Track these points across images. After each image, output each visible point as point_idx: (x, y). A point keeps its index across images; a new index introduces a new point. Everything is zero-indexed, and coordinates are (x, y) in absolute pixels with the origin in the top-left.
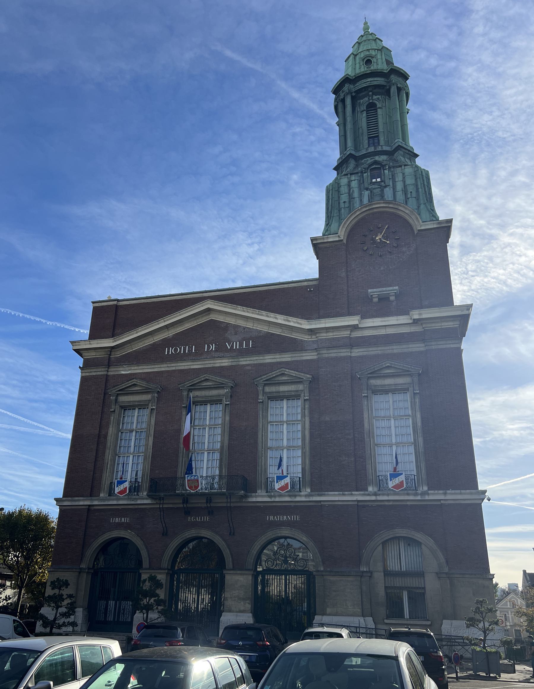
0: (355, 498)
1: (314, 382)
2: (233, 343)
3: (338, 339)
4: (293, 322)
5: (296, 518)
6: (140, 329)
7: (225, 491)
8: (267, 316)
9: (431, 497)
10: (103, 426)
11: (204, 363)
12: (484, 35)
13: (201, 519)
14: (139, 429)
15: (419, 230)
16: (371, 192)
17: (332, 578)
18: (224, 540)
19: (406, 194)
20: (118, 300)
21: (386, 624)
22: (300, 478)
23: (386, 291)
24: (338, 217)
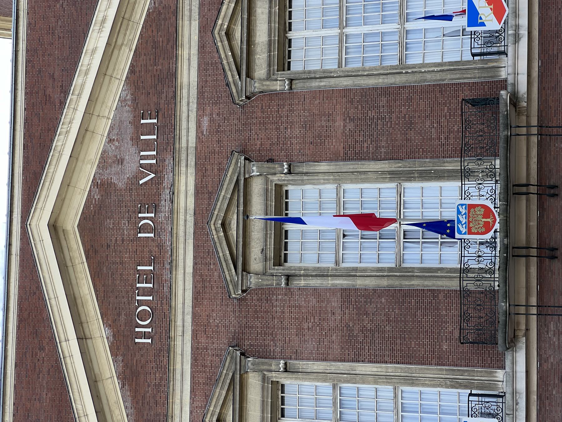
2: (141, 166)
7: (498, 162)
11: (181, 239)
22: (471, 395)
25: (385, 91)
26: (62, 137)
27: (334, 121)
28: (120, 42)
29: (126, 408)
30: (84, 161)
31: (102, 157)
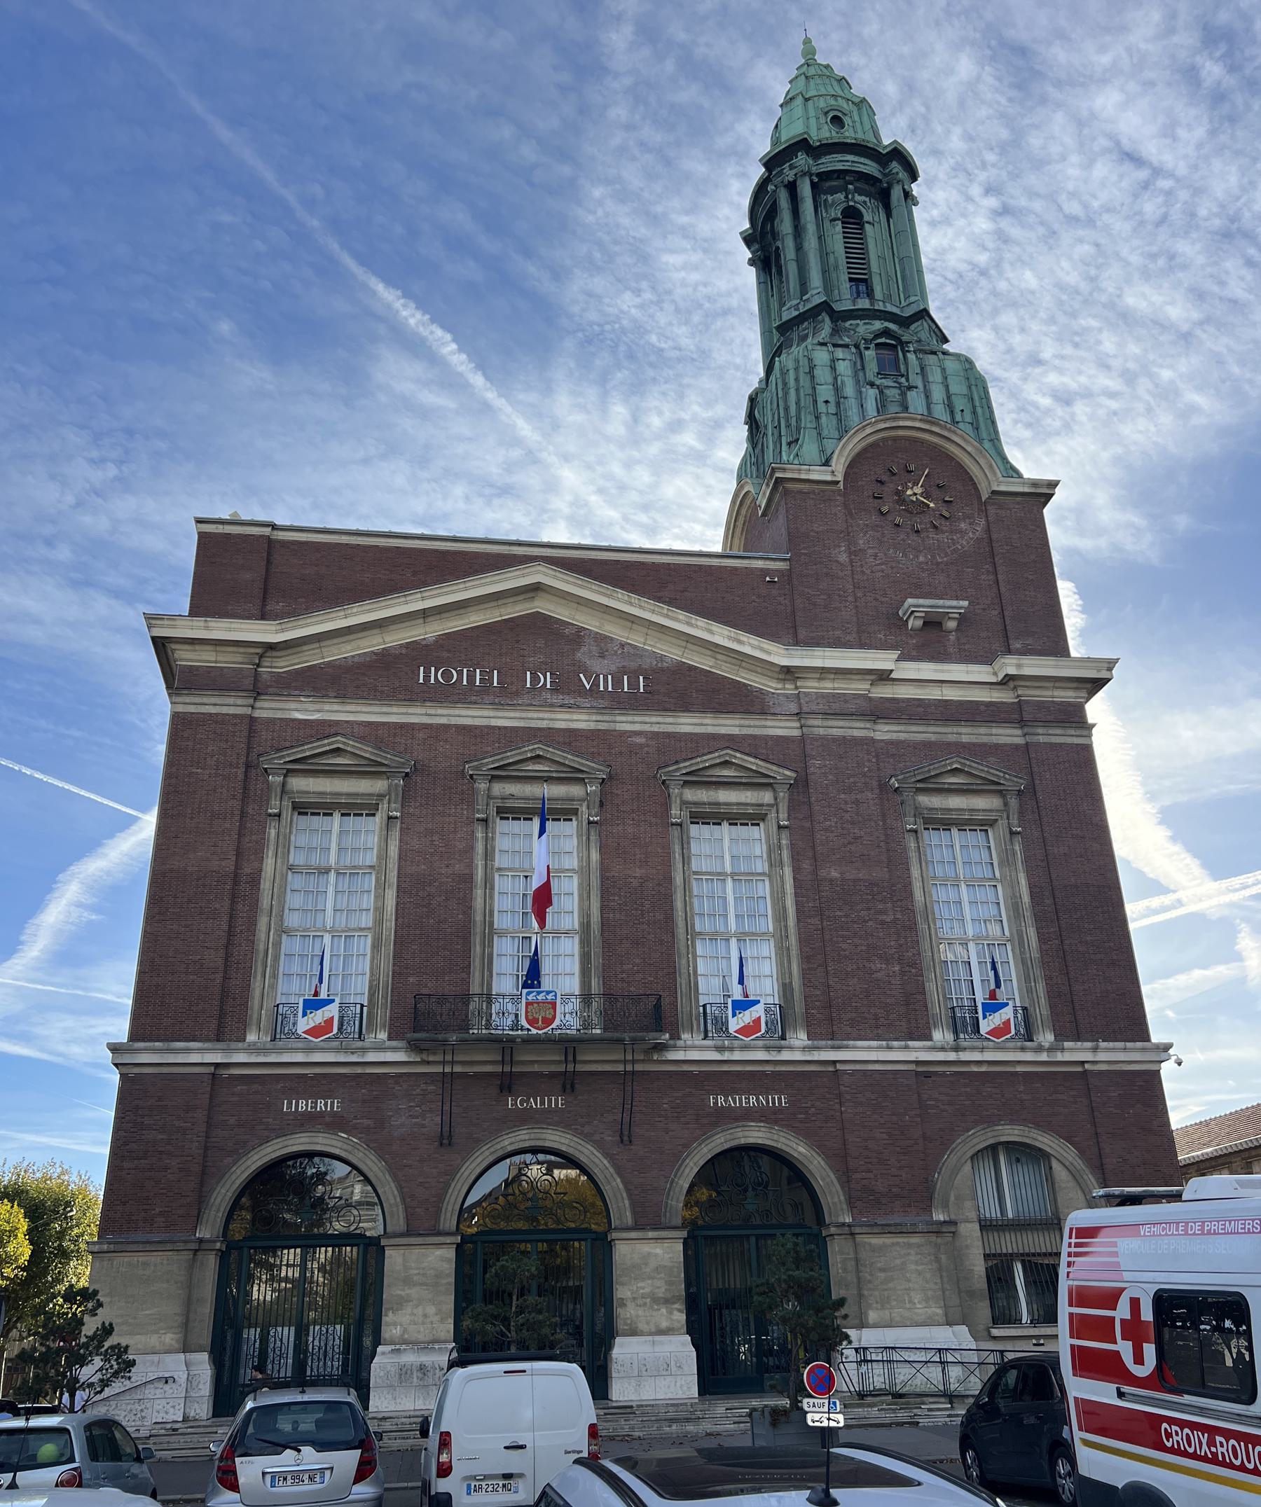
0: (912, 1056)
1: (800, 786)
2: (598, 676)
3: (843, 698)
4: (750, 645)
6: (355, 608)
7: (598, 1031)
8: (689, 624)
9: (1067, 1057)
10: (247, 851)
11: (524, 715)
12: (629, 127)
13: (542, 1103)
14: (346, 867)
15: (994, 492)
16: (881, 392)
17: (876, 1241)
18: (607, 1155)
19: (952, 412)
20: (274, 527)
21: (995, 1338)
24: (814, 433)
27: (640, 867)
28: (719, 656)
31: (606, 637)
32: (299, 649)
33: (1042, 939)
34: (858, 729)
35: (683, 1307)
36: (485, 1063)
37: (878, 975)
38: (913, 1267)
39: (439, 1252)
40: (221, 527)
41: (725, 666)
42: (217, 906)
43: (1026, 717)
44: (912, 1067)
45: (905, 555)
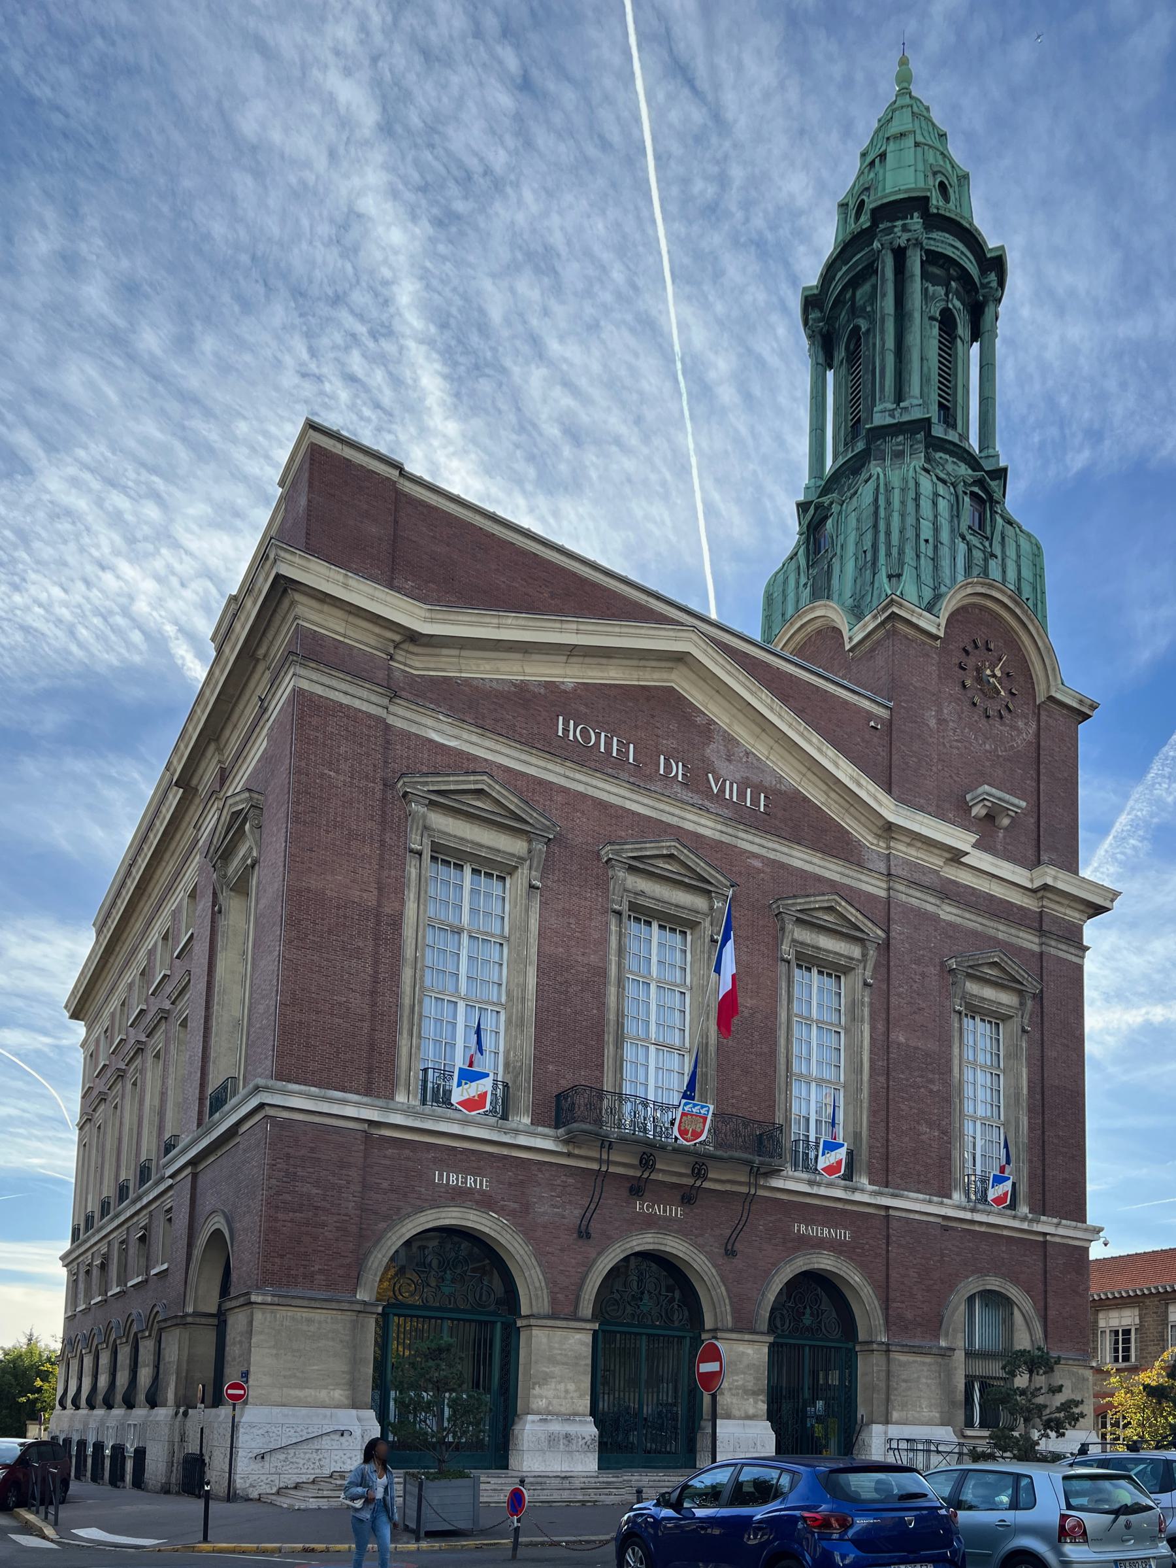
2: (724, 781)
5: (844, 1235)
6: (511, 618)
8: (820, 750)
13: (665, 1211)
15: (1051, 699)
17: (903, 1358)
18: (715, 1266)
23: (1007, 802)
25: (773, 1052)
26: (769, 701)
27: (751, 998)
28: (833, 795)
29: (491, 680)
30: (734, 716)
32: (437, 651)
33: (1031, 1129)
34: (930, 904)
35: (765, 1399)
36: (623, 1163)
37: (923, 1137)
38: (924, 1380)
39: (578, 1336)
40: (339, 446)
41: (834, 806)
42: (360, 944)
43: (1045, 927)
44: (939, 1220)
45: (976, 739)
